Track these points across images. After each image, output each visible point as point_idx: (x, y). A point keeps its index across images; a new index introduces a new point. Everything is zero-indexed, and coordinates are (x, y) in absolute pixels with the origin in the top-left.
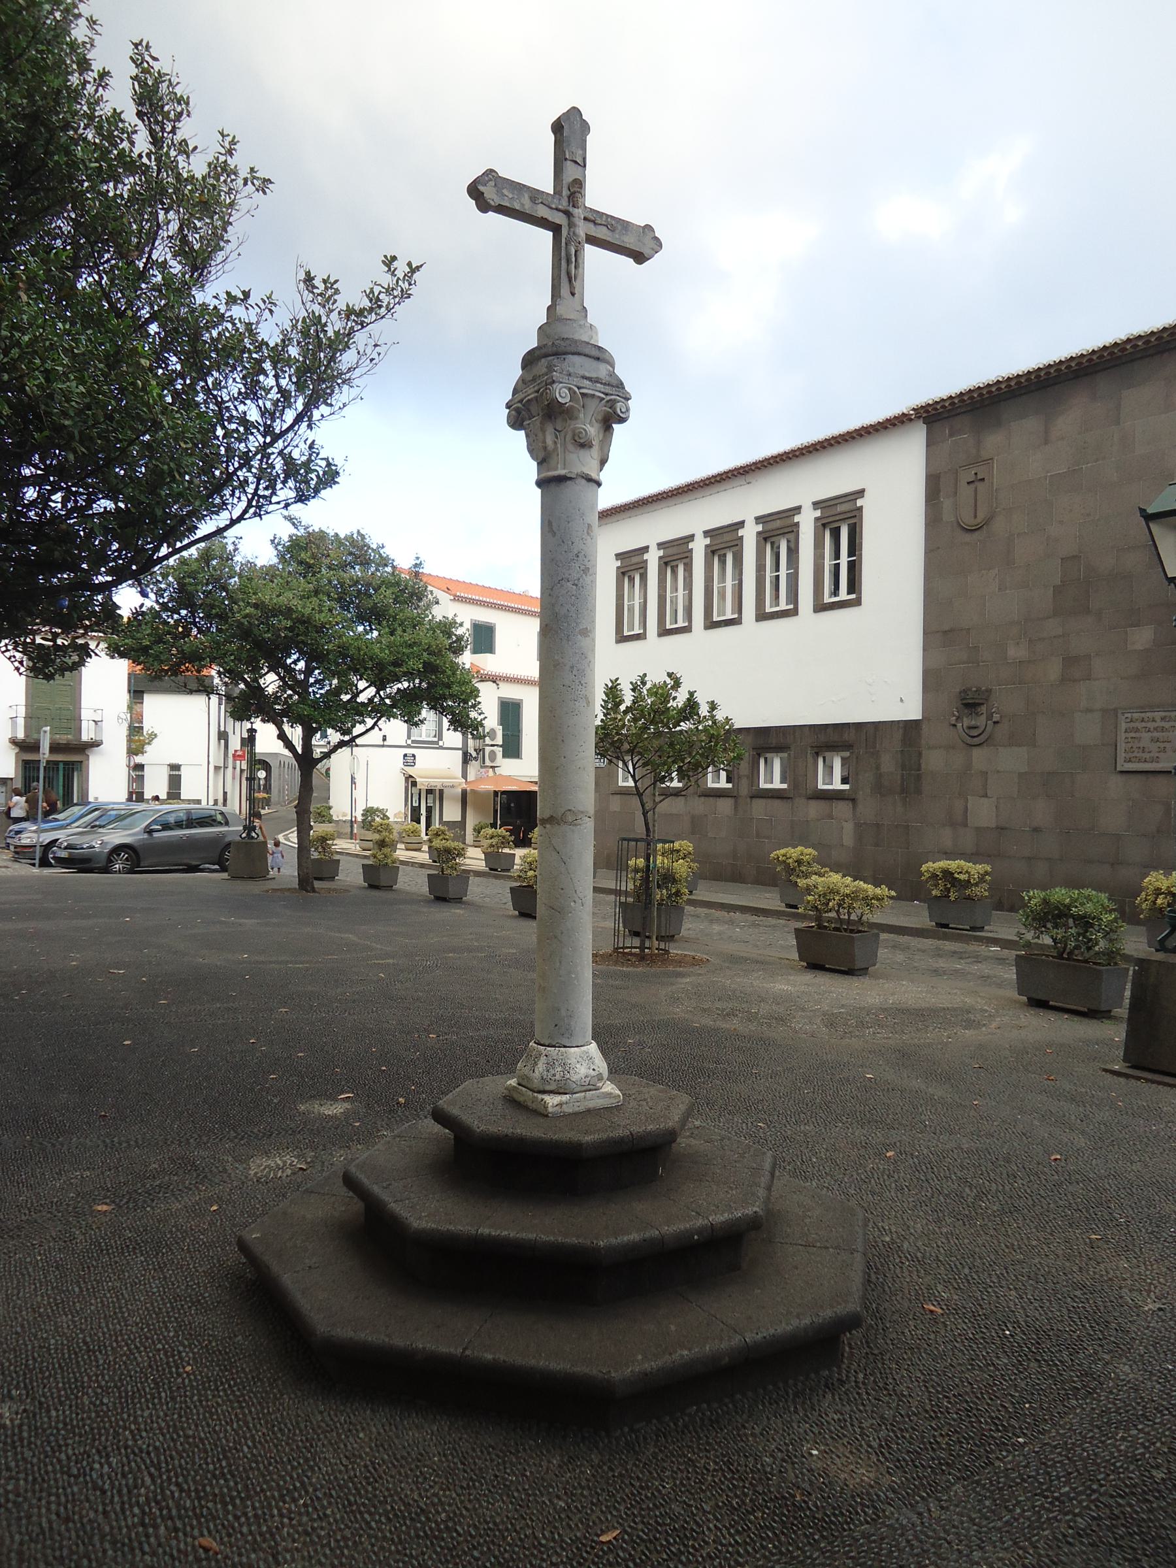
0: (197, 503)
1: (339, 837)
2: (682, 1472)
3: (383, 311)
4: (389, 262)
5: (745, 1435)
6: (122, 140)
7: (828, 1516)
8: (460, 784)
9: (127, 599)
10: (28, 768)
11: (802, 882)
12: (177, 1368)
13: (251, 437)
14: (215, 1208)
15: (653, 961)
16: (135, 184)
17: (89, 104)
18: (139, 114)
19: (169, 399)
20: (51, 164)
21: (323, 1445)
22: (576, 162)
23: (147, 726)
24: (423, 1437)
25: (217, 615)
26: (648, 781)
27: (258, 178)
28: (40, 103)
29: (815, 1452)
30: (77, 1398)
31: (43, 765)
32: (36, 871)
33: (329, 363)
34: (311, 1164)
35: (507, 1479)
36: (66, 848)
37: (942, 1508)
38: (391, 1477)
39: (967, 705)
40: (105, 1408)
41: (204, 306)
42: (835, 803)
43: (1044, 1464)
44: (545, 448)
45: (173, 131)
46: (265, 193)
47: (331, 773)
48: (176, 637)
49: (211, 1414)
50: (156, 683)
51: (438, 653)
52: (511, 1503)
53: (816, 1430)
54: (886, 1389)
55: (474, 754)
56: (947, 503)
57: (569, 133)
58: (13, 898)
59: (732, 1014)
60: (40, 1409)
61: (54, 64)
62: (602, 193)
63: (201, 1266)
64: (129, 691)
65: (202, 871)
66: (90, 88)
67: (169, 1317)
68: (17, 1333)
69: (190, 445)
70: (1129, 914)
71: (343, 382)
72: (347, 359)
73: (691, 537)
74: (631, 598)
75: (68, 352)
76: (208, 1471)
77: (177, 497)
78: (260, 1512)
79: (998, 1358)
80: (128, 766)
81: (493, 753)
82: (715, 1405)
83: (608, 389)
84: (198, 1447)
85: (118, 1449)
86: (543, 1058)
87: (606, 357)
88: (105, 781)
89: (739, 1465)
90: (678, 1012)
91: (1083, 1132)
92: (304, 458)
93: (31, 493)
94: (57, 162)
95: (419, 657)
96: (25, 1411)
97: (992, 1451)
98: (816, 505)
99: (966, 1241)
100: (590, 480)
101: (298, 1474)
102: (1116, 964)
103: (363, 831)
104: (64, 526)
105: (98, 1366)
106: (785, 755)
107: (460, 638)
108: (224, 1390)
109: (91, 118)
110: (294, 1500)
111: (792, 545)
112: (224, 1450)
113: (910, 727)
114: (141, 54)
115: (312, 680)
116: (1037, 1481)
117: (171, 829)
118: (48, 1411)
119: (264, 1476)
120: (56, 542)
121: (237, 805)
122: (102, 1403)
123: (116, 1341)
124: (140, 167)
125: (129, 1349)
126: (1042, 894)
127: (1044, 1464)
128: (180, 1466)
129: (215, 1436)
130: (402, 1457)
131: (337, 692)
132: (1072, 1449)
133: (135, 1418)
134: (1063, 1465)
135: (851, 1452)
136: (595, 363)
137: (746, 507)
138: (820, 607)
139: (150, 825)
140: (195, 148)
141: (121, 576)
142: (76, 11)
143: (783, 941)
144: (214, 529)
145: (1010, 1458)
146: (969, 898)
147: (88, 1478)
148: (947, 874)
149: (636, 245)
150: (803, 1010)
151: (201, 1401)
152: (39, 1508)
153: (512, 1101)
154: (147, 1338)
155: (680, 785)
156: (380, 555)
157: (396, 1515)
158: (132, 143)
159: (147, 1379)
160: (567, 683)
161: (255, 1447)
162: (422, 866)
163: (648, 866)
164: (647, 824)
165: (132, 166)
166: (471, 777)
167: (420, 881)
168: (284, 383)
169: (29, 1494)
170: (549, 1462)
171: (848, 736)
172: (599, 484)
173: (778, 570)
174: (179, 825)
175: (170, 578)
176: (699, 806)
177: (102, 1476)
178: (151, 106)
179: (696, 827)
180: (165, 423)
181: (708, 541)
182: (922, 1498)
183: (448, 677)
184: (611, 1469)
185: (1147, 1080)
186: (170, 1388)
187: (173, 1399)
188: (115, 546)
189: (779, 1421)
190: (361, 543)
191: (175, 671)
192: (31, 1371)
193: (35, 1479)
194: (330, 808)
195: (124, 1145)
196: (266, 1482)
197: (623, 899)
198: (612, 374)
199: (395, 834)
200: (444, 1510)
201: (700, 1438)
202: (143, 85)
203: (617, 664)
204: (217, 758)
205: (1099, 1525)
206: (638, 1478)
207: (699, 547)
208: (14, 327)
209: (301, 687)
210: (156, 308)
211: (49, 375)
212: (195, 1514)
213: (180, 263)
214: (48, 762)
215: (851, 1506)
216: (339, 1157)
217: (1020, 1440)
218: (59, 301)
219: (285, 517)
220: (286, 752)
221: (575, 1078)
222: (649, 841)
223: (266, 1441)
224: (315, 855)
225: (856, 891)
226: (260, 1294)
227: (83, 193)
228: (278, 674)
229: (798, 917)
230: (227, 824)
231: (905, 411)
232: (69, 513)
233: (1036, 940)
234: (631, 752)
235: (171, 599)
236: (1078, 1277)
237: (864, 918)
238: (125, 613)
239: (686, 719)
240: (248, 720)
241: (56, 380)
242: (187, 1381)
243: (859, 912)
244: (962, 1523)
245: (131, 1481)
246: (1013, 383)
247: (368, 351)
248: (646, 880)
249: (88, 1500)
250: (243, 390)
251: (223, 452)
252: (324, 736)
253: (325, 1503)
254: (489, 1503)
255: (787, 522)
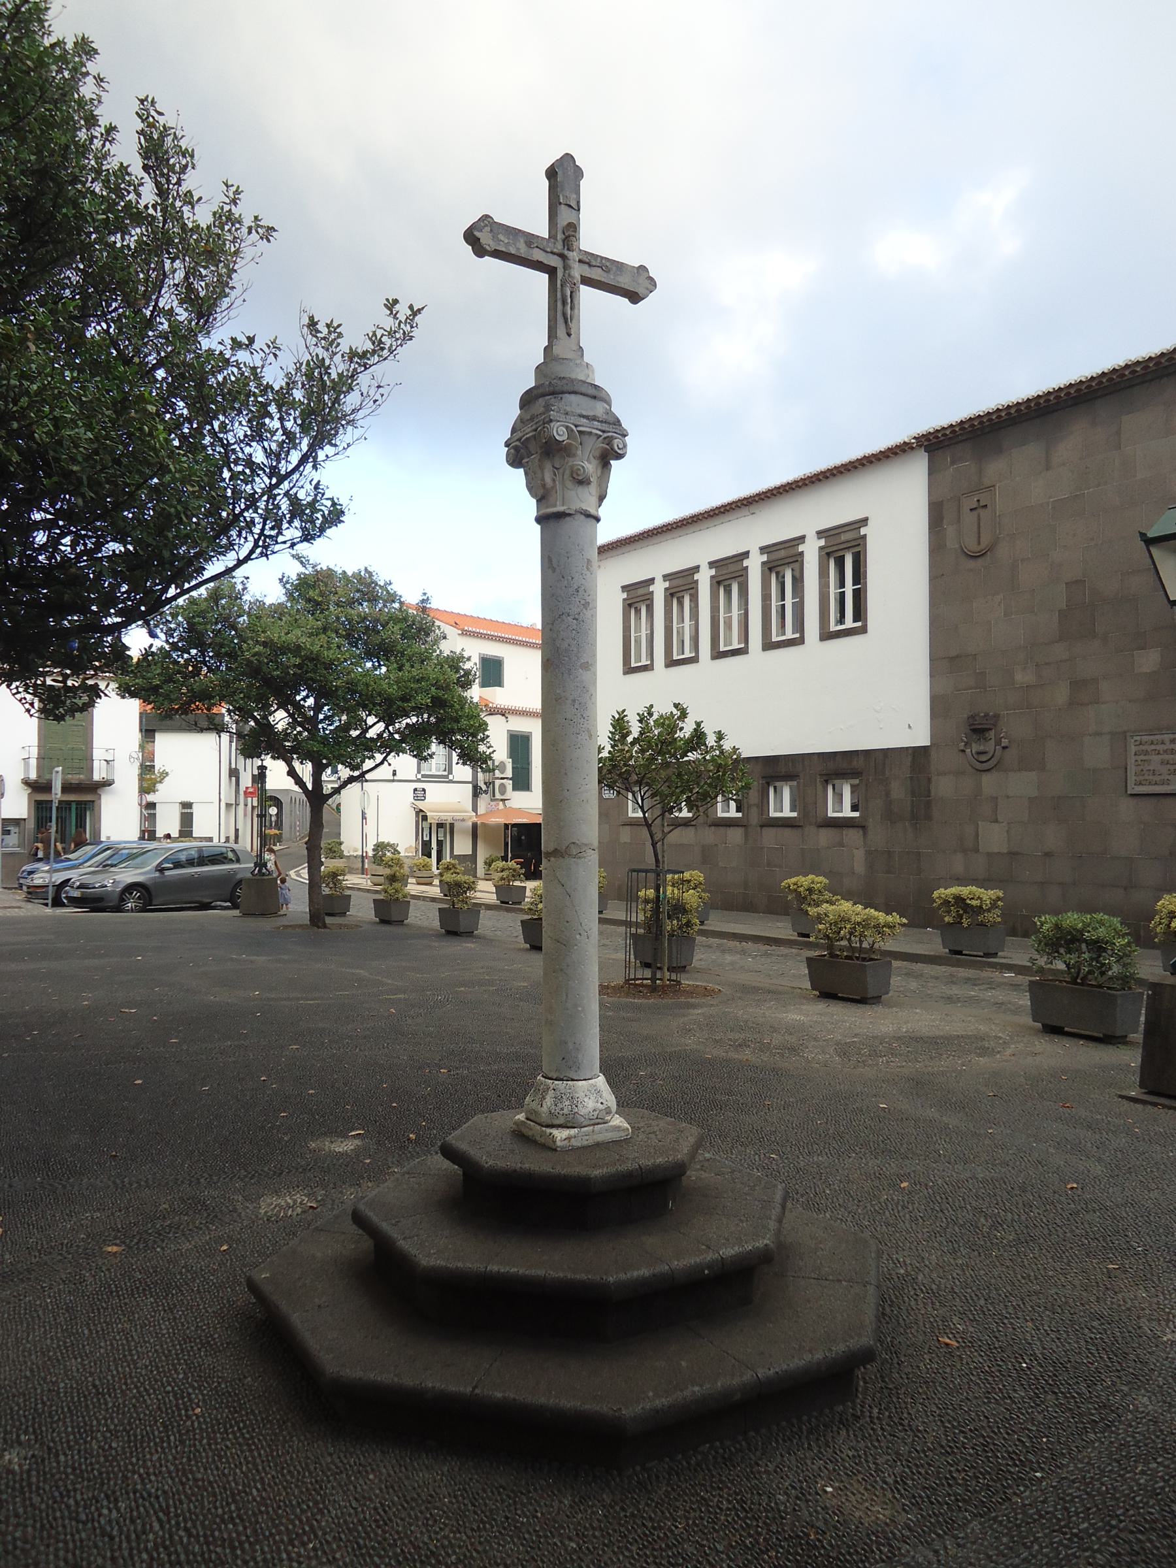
0: (204, 545)
1: (350, 872)
2: (694, 1510)
3: (385, 353)
4: (391, 305)
5: (759, 1472)
6: (129, 193)
7: (843, 1555)
8: (471, 817)
9: (137, 640)
10: (41, 809)
11: (812, 911)
12: (187, 1410)
13: (257, 479)
14: (225, 1247)
15: (664, 992)
16: (142, 234)
17: (96, 158)
18: (146, 168)
19: (176, 443)
20: (59, 217)
21: (333, 1488)
22: (570, 206)
23: (159, 765)
24: (433, 1478)
25: (226, 654)
26: (658, 812)
27: (262, 227)
28: (47, 160)
29: (829, 1489)
30: (86, 1442)
31: (55, 805)
32: (49, 911)
33: (333, 404)
34: (322, 1203)
35: (518, 1521)
36: (78, 888)
37: (959, 1545)
38: (402, 1519)
39: (975, 731)
40: (113, 1452)
41: (210, 352)
42: (845, 831)
43: (1062, 1499)
44: (544, 486)
45: (179, 183)
46: (269, 241)
47: (342, 808)
48: (186, 676)
49: (220, 1457)
50: (168, 722)
51: (446, 688)
52: (522, 1545)
53: (830, 1467)
54: (902, 1424)
55: (484, 788)
56: (950, 531)
57: (563, 179)
58: (26, 938)
59: (743, 1045)
60: (49, 1454)
61: (62, 119)
62: (597, 235)
63: (210, 1306)
64: (141, 730)
65: (214, 908)
66: (97, 143)
67: (178, 1359)
68: (26, 1377)
69: (197, 488)
70: (1142, 938)
71: (347, 424)
72: (351, 401)
73: (697, 569)
74: (638, 630)
75: (77, 399)
76: (217, 1516)
77: (184, 539)
78: (269, 1556)
79: (1015, 1391)
80: (140, 805)
81: (503, 786)
82: (728, 1443)
83: (605, 427)
84: (206, 1490)
85: (127, 1493)
86: (551, 1093)
87: (603, 395)
88: (118, 820)
89: (752, 1503)
90: (690, 1043)
91: (1100, 1160)
92: (309, 499)
93: (41, 538)
94: (65, 215)
95: (427, 691)
96: (33, 1456)
97: (1010, 1486)
98: (820, 534)
99: (982, 1272)
100: (588, 516)
101: (307, 1518)
102: (1130, 988)
103: (374, 866)
104: (73, 570)
105: (107, 1410)
106: (795, 783)
107: (468, 673)
108: (234, 1433)
109: (98, 172)
110: (304, 1544)
111: (797, 574)
112: (233, 1494)
113: (918, 753)
114: (146, 109)
115: (321, 717)
116: (1056, 1517)
117: (183, 867)
118: (57, 1455)
119: (273, 1520)
120: (67, 585)
121: (248, 843)
122: (110, 1447)
123: (126, 1384)
124: (146, 218)
125: (139, 1392)
126: (1054, 919)
127: (1062, 1499)
128: (189, 1511)
129: (225, 1480)
130: (412, 1499)
131: (346, 728)
132: (1090, 1483)
133: (144, 1461)
134: (1082, 1500)
135: (866, 1489)
136: (591, 402)
137: (750, 537)
138: (827, 635)
139: (161, 863)
140: (200, 199)
141: (130, 617)
142: (84, 70)
143: (794, 970)
144: (223, 569)
145: (1027, 1493)
146: (982, 924)
147: (96, 1525)
148: (959, 900)
149: (631, 285)
150: (815, 1039)
151: (210, 1445)
152: (47, 1555)
153: (520, 1136)
154: (156, 1381)
155: (690, 815)
156: (388, 592)
157: (406, 1559)
158: (139, 195)
159: (156, 1422)
160: (569, 716)
161: (265, 1490)
162: (433, 900)
163: (658, 897)
164: (656, 855)
165: (139, 217)
166: (481, 811)
167: (431, 915)
168: (289, 425)
169: (37, 1541)
170: (561, 1502)
171: (858, 764)
172: (598, 520)
173: (783, 599)
174: (190, 863)
175: (180, 618)
176: (709, 836)
177: (110, 1521)
178: (156, 159)
179: (706, 858)
180: (171, 466)
181: (713, 572)
182: (938, 1535)
183: (456, 711)
184: (623, 1509)
185: (1164, 1106)
186: (179, 1432)
187: (182, 1442)
188: (125, 588)
189: (793, 1458)
190: (369, 581)
191: (185, 710)
192: (40, 1415)
193: (43, 1526)
194: (341, 844)
195: (135, 1185)
196: (275, 1526)
197: (633, 930)
198: (609, 412)
199: (406, 866)
200: (455, 1553)
201: (713, 1476)
202: (149, 139)
203: (619, 696)
204: (228, 795)
205: (1118, 1561)
206: (650, 1517)
207: (704, 578)
208: (23, 376)
209: (311, 723)
210: (163, 354)
211: (57, 422)
212: (204, 1559)
213: (186, 310)
214: (60, 802)
215: (865, 1544)
216: (349, 1195)
217: (1038, 1474)
218: (68, 349)
219: (293, 556)
220: (297, 788)
221: (583, 1111)
222: (658, 873)
223: (275, 1484)
224: (326, 891)
225: (867, 919)
226: (270, 1335)
227: (91, 244)
228: (287, 711)
229: (810, 946)
230: (238, 861)
231: (907, 440)
232: (79, 556)
233: (1049, 966)
234: (639, 783)
235: (181, 639)
236: (1096, 1307)
237: (876, 946)
238: (135, 653)
239: (693, 749)
240: (259, 757)
241: (64, 427)
242: (196, 1424)
243: (870, 940)
244: (979, 1560)
245: (139, 1527)
246: (1013, 411)
247: (372, 393)
248: (656, 911)
249: (96, 1547)
250: (249, 433)
251: (229, 494)
252: (335, 772)
253: (335, 1546)
254: (499, 1544)
255: (791, 552)
